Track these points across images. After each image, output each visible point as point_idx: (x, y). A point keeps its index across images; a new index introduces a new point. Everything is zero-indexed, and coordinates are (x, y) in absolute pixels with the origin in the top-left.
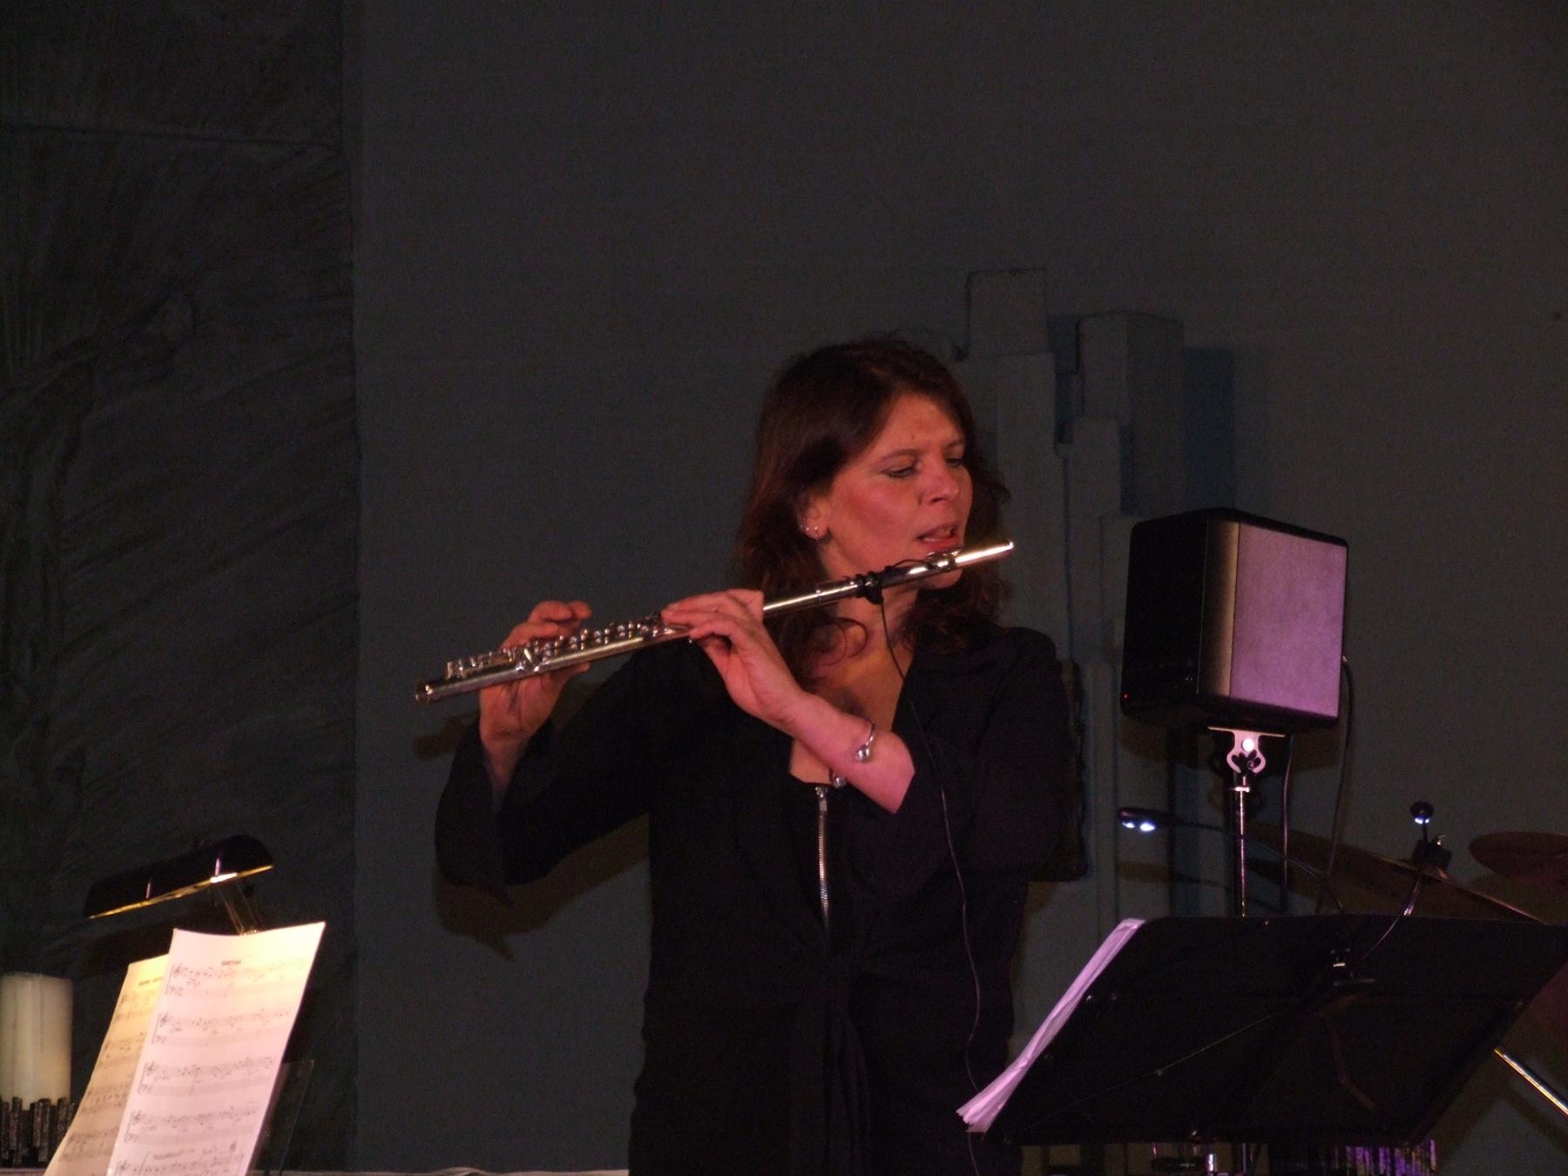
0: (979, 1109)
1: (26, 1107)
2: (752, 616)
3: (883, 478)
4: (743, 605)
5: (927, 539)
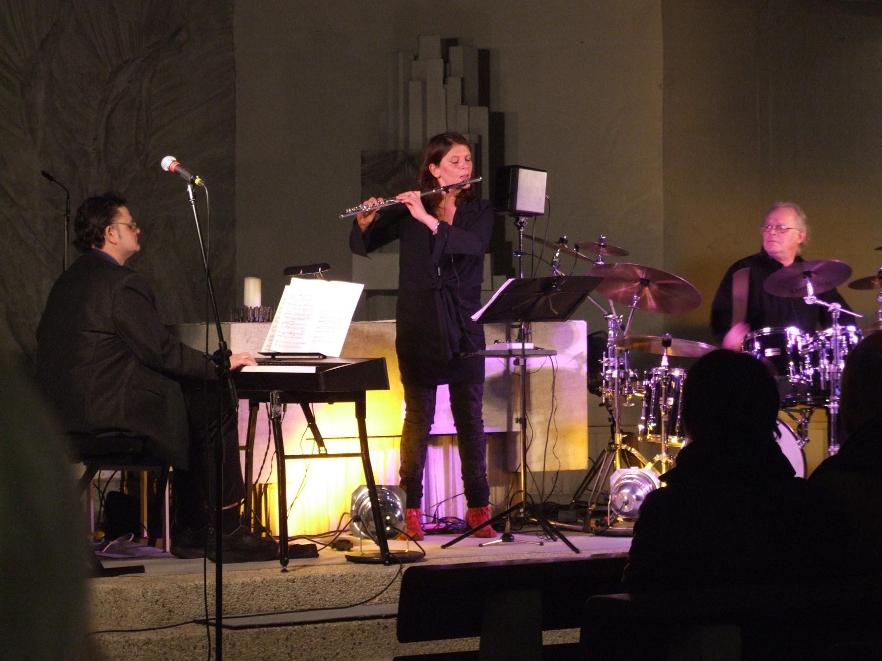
0: (476, 317)
1: (253, 308)
2: (417, 197)
3: (450, 163)
4: (416, 194)
5: (534, 484)
